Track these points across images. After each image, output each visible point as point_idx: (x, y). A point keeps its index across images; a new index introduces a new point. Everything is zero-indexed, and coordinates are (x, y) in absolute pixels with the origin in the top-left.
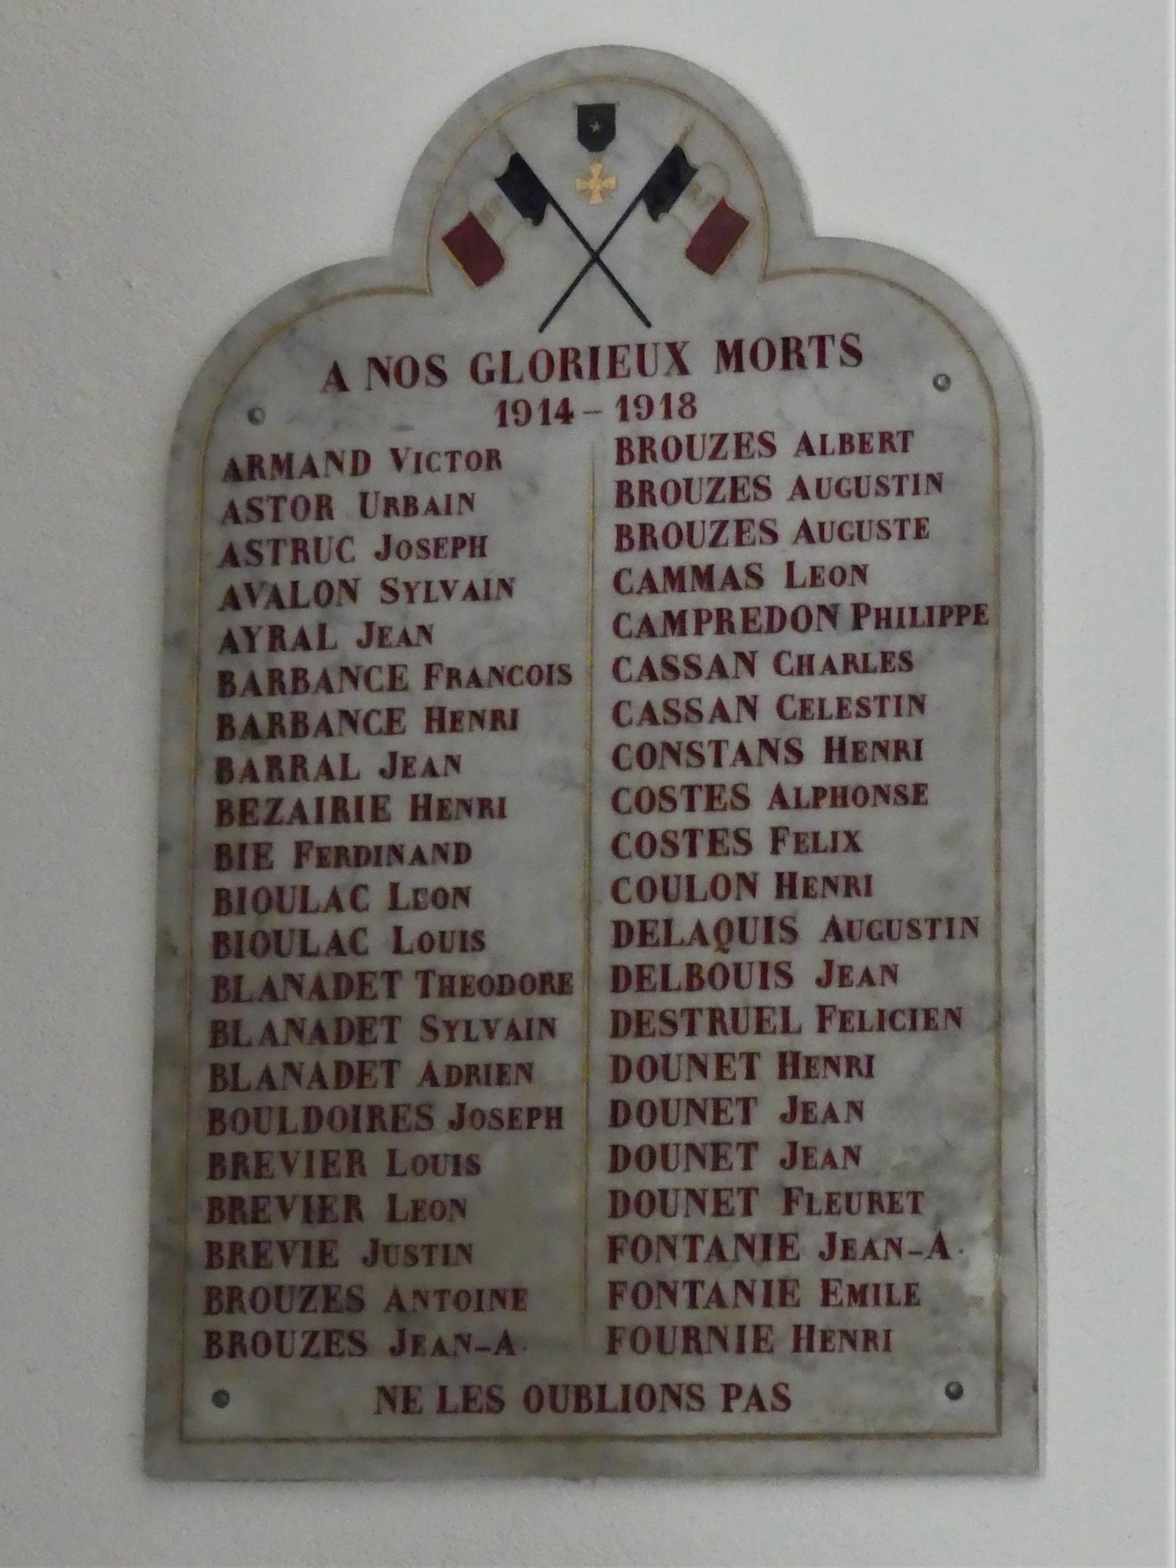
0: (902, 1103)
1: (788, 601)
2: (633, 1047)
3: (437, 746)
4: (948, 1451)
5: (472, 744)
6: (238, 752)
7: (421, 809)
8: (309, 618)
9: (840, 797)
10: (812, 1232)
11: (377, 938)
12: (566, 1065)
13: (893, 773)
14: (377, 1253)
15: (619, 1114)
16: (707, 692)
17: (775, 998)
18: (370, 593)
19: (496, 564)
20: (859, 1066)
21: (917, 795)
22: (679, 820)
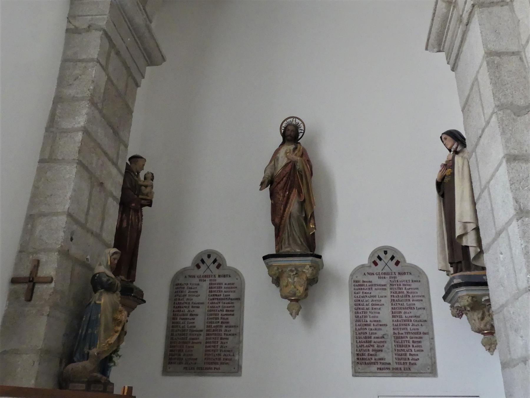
0: (231, 342)
1: (223, 297)
2: (208, 337)
3: (192, 309)
4: (361, 374)
5: (195, 309)
6: (175, 309)
7: (191, 315)
8: (182, 298)
9: (227, 315)
10: (222, 354)
11: (186, 326)
12: (202, 338)
13: (232, 313)
14: (184, 355)
15: (206, 343)
16: (216, 305)
17: (220, 332)
18: (187, 296)
19: (198, 293)
20: (227, 339)
21: (233, 315)
22: (213, 316)
